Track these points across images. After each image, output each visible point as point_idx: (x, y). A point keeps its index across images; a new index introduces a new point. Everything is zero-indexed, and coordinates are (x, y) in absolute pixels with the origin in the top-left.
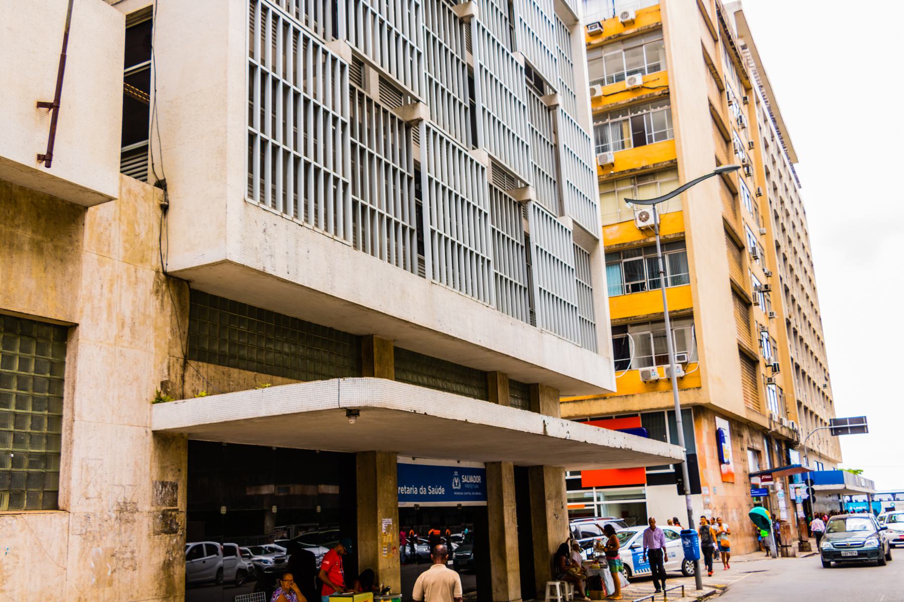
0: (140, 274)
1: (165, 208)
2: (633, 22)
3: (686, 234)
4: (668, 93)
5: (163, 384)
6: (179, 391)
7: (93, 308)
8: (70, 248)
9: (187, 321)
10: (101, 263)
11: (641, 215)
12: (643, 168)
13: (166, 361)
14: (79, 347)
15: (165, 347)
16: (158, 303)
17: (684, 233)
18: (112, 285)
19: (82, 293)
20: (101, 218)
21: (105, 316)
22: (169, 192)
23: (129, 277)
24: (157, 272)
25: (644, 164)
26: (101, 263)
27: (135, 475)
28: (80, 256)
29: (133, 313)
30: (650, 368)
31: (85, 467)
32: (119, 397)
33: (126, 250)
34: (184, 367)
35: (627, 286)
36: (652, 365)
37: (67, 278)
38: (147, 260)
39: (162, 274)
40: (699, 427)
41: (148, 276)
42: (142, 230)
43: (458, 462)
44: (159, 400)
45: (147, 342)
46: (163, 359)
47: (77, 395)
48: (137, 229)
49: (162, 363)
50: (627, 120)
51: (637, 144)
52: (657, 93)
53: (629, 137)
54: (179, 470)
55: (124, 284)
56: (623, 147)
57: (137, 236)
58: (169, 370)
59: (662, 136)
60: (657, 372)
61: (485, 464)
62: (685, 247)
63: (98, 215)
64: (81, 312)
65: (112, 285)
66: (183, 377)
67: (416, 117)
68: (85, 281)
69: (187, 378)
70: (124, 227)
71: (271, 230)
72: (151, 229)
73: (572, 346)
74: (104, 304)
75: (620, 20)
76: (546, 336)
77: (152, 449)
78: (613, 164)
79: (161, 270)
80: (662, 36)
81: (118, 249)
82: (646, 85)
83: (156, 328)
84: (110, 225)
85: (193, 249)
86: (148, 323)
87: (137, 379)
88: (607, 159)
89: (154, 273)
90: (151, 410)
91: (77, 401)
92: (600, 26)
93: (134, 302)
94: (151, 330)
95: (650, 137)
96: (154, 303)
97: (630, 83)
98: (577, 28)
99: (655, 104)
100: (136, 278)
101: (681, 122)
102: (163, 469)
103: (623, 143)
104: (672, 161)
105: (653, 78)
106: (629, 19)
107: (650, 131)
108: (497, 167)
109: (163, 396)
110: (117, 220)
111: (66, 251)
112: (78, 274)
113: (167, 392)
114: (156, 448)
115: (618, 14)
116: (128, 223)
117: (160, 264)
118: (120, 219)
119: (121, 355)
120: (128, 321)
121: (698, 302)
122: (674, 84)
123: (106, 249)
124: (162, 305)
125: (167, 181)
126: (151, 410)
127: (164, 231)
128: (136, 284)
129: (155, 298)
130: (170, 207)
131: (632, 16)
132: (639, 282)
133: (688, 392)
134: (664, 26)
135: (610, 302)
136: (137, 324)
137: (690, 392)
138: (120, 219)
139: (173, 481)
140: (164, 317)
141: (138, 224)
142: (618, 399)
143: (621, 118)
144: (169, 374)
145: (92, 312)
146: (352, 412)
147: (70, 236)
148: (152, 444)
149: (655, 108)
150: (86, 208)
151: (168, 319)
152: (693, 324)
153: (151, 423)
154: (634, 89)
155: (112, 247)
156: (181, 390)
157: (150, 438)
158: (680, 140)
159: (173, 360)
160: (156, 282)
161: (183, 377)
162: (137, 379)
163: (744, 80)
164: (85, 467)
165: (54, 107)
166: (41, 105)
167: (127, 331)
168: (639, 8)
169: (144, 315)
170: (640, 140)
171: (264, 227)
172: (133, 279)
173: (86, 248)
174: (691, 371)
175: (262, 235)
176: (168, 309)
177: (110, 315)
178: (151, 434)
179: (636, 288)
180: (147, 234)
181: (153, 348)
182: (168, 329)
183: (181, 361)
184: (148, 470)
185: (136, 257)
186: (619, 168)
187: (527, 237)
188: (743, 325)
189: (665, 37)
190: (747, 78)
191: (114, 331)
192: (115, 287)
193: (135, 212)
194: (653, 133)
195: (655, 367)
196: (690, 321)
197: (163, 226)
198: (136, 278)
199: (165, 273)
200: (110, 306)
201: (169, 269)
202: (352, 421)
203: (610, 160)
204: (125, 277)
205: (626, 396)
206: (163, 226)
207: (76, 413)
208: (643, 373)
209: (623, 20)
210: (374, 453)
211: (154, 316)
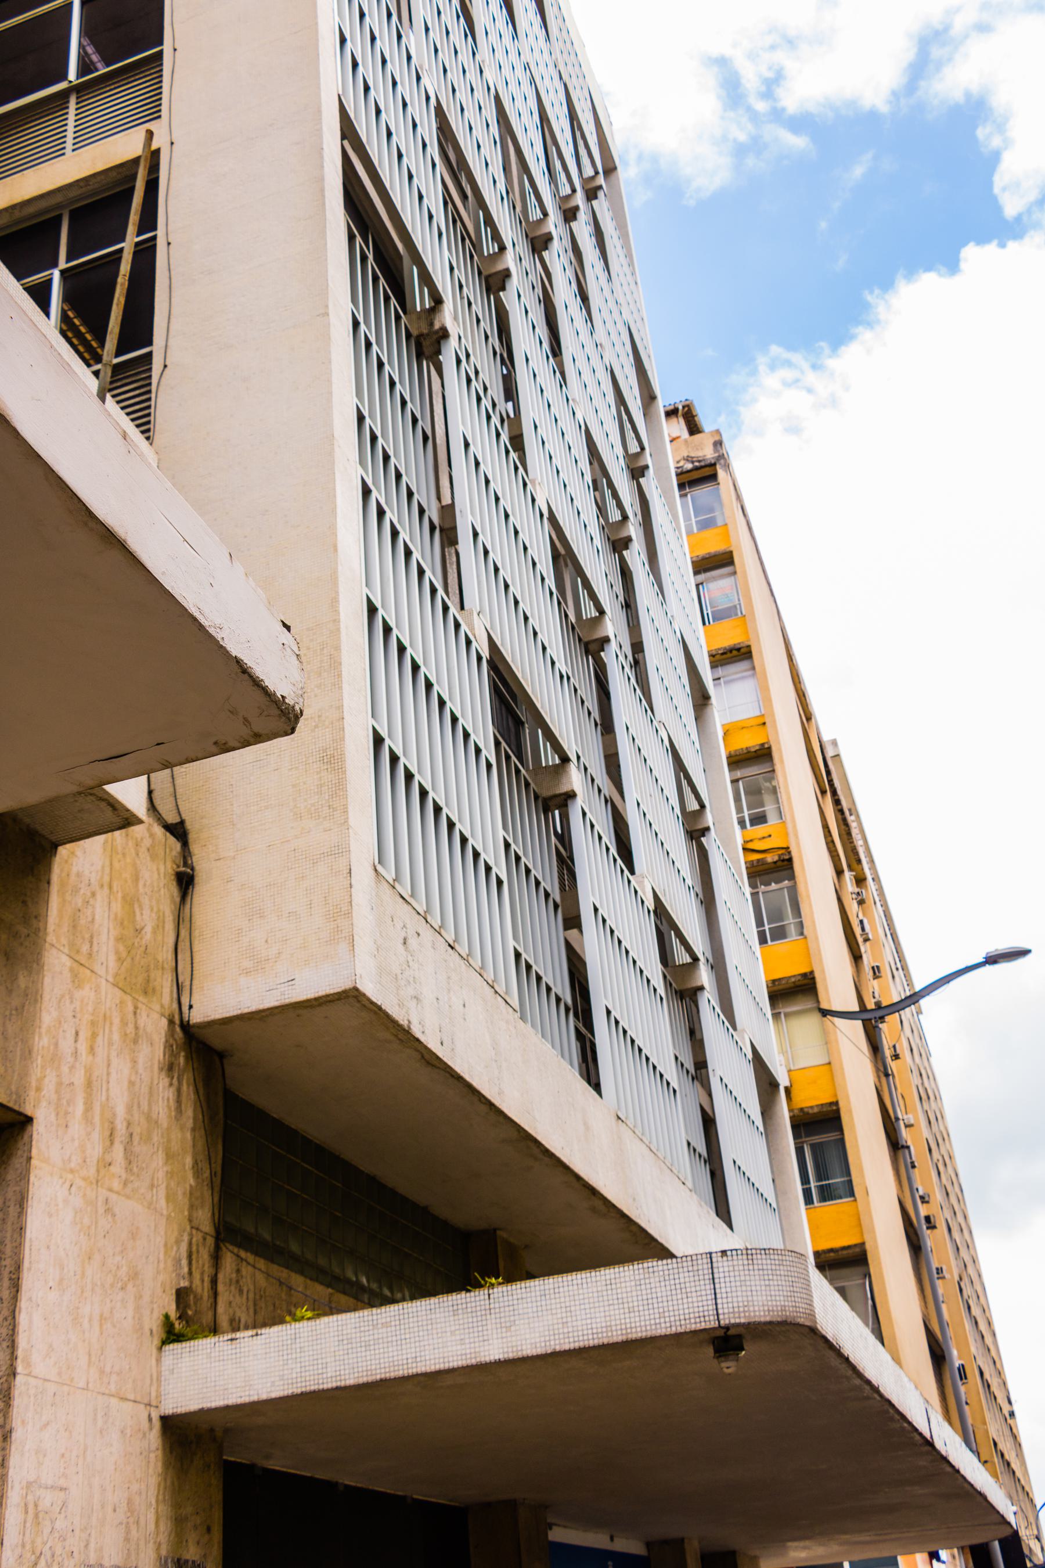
0: (143, 1020)
1: (185, 881)
3: (841, 1105)
4: (790, 860)
5: (182, 1296)
6: (207, 1318)
7: (59, 1084)
8: (24, 931)
9: (220, 1147)
10: (77, 981)
13: (186, 1238)
14: (32, 1178)
15: (183, 1201)
16: (171, 1094)
17: (837, 1103)
18: (94, 1035)
19: (42, 1042)
20: (78, 875)
21: (79, 1108)
22: (195, 848)
23: (124, 1023)
24: (171, 1022)
26: (77, 981)
27: (127, 1540)
28: (39, 954)
29: (129, 1109)
31: (31, 1507)
32: (102, 1319)
33: (120, 960)
34: (216, 1258)
37: (16, 1002)
38: (154, 990)
39: (178, 1029)
41: (155, 1027)
42: (146, 919)
43: (612, 1539)
44: (172, 1335)
45: (152, 1186)
46: (181, 1231)
47: (23, 1303)
48: (138, 917)
49: (178, 1242)
52: (770, 858)
54: (209, 1530)
55: (116, 1037)
57: (138, 931)
58: (190, 1264)
61: (649, 1545)
62: (841, 1130)
63: (74, 870)
64: (38, 1089)
65: (94, 1035)
66: (214, 1281)
67: (564, 789)
68: (47, 1017)
69: (221, 1288)
70: (117, 907)
71: (413, 942)
72: (159, 926)
74: (79, 1078)
77: (160, 1468)
79: (177, 1022)
80: (773, 765)
81: (106, 956)
83: (169, 1156)
84: (93, 894)
86: (155, 1139)
87: (134, 1275)
89: (164, 1022)
90: (158, 1360)
91: (23, 1319)
93: (132, 1083)
94: (160, 1157)
96: (164, 1094)
98: (708, 710)
99: (766, 878)
100: (137, 1028)
102: (179, 1522)
104: (804, 975)
105: (760, 835)
109: (178, 1326)
110: (106, 888)
111: (16, 935)
112: (32, 997)
113: (187, 1321)
114: (167, 1465)
116: (124, 898)
117: (175, 1006)
118: (110, 887)
119: (107, 1211)
120: (121, 1127)
121: (873, 1230)
122: (798, 845)
123: (85, 948)
124: (179, 1101)
125: (188, 825)
126: (158, 1360)
127: (184, 933)
128: (135, 1041)
129: (167, 1081)
130: (197, 880)
134: (774, 749)
135: (807, 1214)
136: (136, 1139)
138: (110, 887)
139: (196, 1558)
140: (182, 1128)
141: (141, 907)
144: (190, 1273)
145: (57, 1092)
146: (727, 1340)
147: (24, 902)
148: (160, 1453)
149: (768, 884)
150: (55, 846)
151: (188, 1135)
152: (868, 1275)
153: (158, 1396)
155: (95, 948)
156: (210, 1314)
157: (154, 1437)
159: (197, 1237)
160: (168, 1046)
161: (214, 1281)
162: (134, 1275)
163: (854, 865)
164: (31, 1507)
167: (118, 1151)
168: (729, 720)
169: (148, 1118)
171: (403, 934)
172: (130, 1029)
173: (51, 938)
175: (401, 948)
176: (189, 1113)
177: (88, 1108)
178: (157, 1424)
180: (154, 932)
181: (163, 1202)
182: (189, 1161)
183: (210, 1241)
184: (152, 1526)
185: (136, 984)
189: (778, 767)
190: (859, 861)
191: (95, 1150)
192: (99, 1039)
193: (136, 878)
194: (767, 927)
196: (860, 1270)
197: (183, 917)
198: (137, 1028)
199: (186, 1027)
200: (89, 1084)
201: (197, 1016)
202: (729, 1367)
204: (116, 1021)
206: (183, 917)
207: (20, 1353)
210: (511, 1506)
211: (165, 1125)
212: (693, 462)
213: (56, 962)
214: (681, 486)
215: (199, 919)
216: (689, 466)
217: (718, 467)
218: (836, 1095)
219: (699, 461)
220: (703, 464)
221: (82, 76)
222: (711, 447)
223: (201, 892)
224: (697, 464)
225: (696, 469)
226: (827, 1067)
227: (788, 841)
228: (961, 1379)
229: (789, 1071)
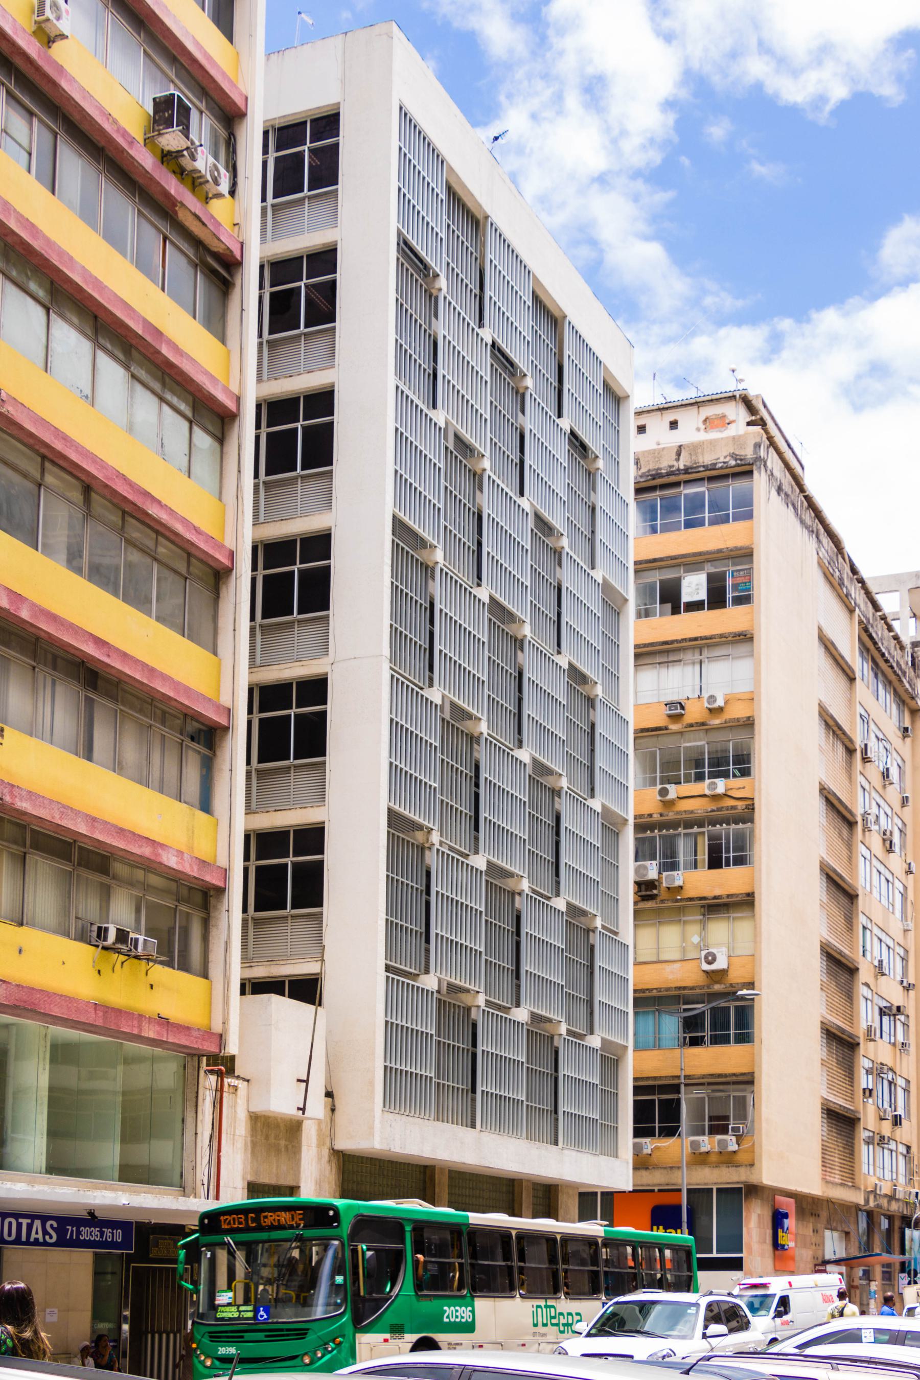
1: (333, 1110)
2: (721, 710)
11: (706, 957)
12: (715, 898)
25: (717, 892)
30: (701, 1138)
35: (685, 1038)
36: (704, 1134)
40: (748, 1211)
41: (326, 1152)
50: (703, 833)
51: (711, 867)
53: (703, 856)
56: (696, 868)
59: (740, 861)
60: (707, 1143)
73: (589, 1156)
75: (706, 705)
76: (566, 1152)
78: (681, 887)
82: (729, 793)
83: (329, 1183)
85: (352, 1141)
88: (674, 880)
92: (682, 708)
95: (728, 859)
96: (328, 1168)
97: (709, 788)
101: (764, 848)
103: (696, 860)
106: (716, 705)
107: (728, 851)
108: (538, 517)
115: (705, 695)
121: (760, 1066)
131: (720, 702)
132: (699, 1034)
133: (739, 1169)
134: (756, 722)
137: (742, 1170)
142: (662, 1171)
143: (696, 829)
154: (716, 797)
158: (760, 870)
165: (307, 1081)
166: (299, 1080)
170: (715, 862)
174: (746, 1145)
176: (334, 1172)
179: (696, 1042)
186: (690, 892)
187: (593, 726)
188: (839, 1073)
195: (705, 1138)
201: (336, 1148)
203: (678, 883)
205: (671, 1168)
208: (692, 1143)
209: (709, 706)
212: (736, 460)
213: (304, 1148)
214: (637, 656)
215: (337, 1121)
216: (733, 463)
217: (754, 468)
218: (753, 977)
219: (741, 460)
220: (743, 463)
221: (292, 289)
222: (752, 448)
223: (337, 1112)
224: (739, 462)
225: (738, 465)
226: (750, 958)
227: (753, 794)
228: (210, 1333)
229: (729, 957)
